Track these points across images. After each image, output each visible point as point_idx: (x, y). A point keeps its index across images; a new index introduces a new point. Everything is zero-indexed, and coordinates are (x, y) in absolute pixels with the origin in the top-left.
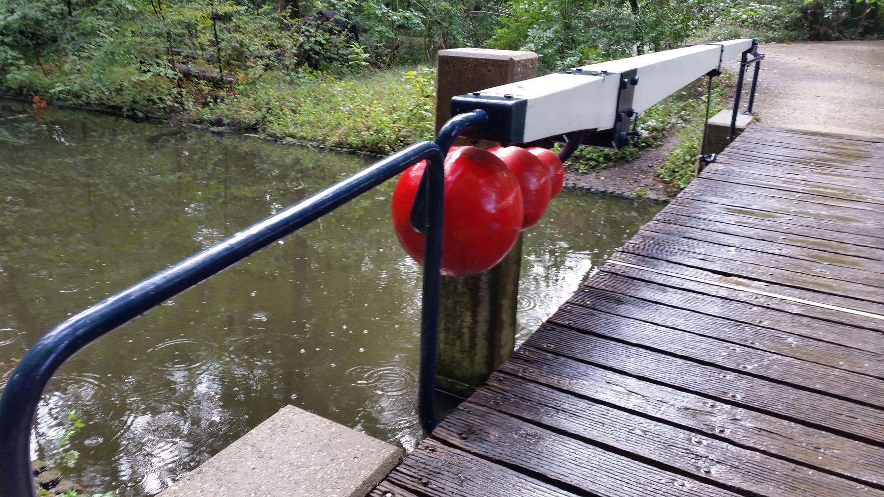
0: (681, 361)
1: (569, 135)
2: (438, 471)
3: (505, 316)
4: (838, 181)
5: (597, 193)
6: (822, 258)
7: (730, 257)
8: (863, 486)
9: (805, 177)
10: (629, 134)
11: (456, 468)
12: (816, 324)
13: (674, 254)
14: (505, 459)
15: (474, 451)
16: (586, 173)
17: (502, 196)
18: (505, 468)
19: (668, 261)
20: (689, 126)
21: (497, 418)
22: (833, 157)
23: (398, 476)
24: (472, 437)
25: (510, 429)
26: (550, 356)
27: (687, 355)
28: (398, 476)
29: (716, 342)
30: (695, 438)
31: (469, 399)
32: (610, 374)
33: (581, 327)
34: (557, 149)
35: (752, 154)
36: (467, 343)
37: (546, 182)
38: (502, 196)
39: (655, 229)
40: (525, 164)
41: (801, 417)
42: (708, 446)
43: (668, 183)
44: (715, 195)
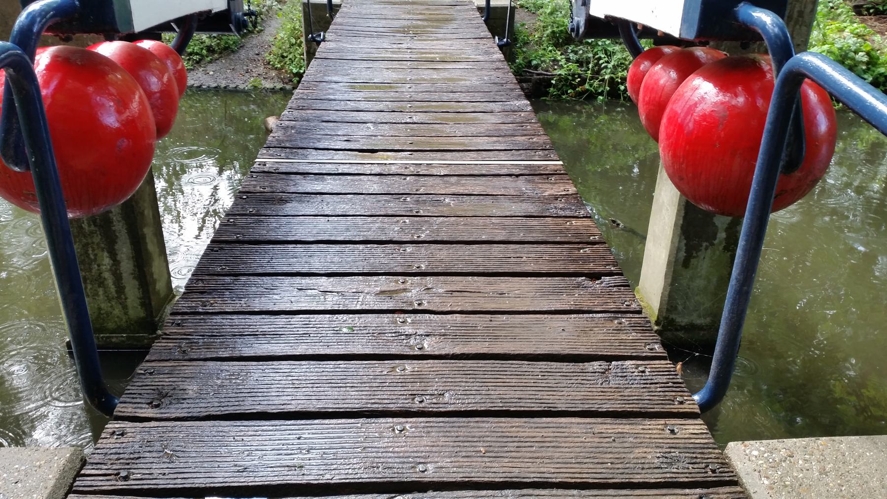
0: (361, 247)
1: (180, 21)
2: (136, 456)
3: (151, 247)
4: (437, 45)
5: (209, 89)
6: (448, 119)
7: (371, 134)
8: (546, 316)
9: (409, 46)
10: (245, 14)
11: (158, 444)
12: (463, 180)
13: (319, 140)
14: (214, 411)
15: (174, 416)
16: (191, 70)
17: (123, 104)
18: (216, 423)
19: (316, 149)
20: (285, 7)
21: (190, 369)
22: (425, 23)
23: (88, 481)
24: (166, 401)
25: (210, 376)
26: (228, 279)
27: (365, 239)
28: (88, 481)
29: (386, 219)
30: (399, 318)
31: (147, 358)
32: (298, 280)
33: (252, 238)
34: (170, 38)
35: (356, 28)
36: (112, 289)
37: (169, 80)
38: (123, 104)
39: (292, 118)
40: (137, 63)
41: (481, 269)
42: (413, 323)
43: (280, 69)
44: (336, 74)
